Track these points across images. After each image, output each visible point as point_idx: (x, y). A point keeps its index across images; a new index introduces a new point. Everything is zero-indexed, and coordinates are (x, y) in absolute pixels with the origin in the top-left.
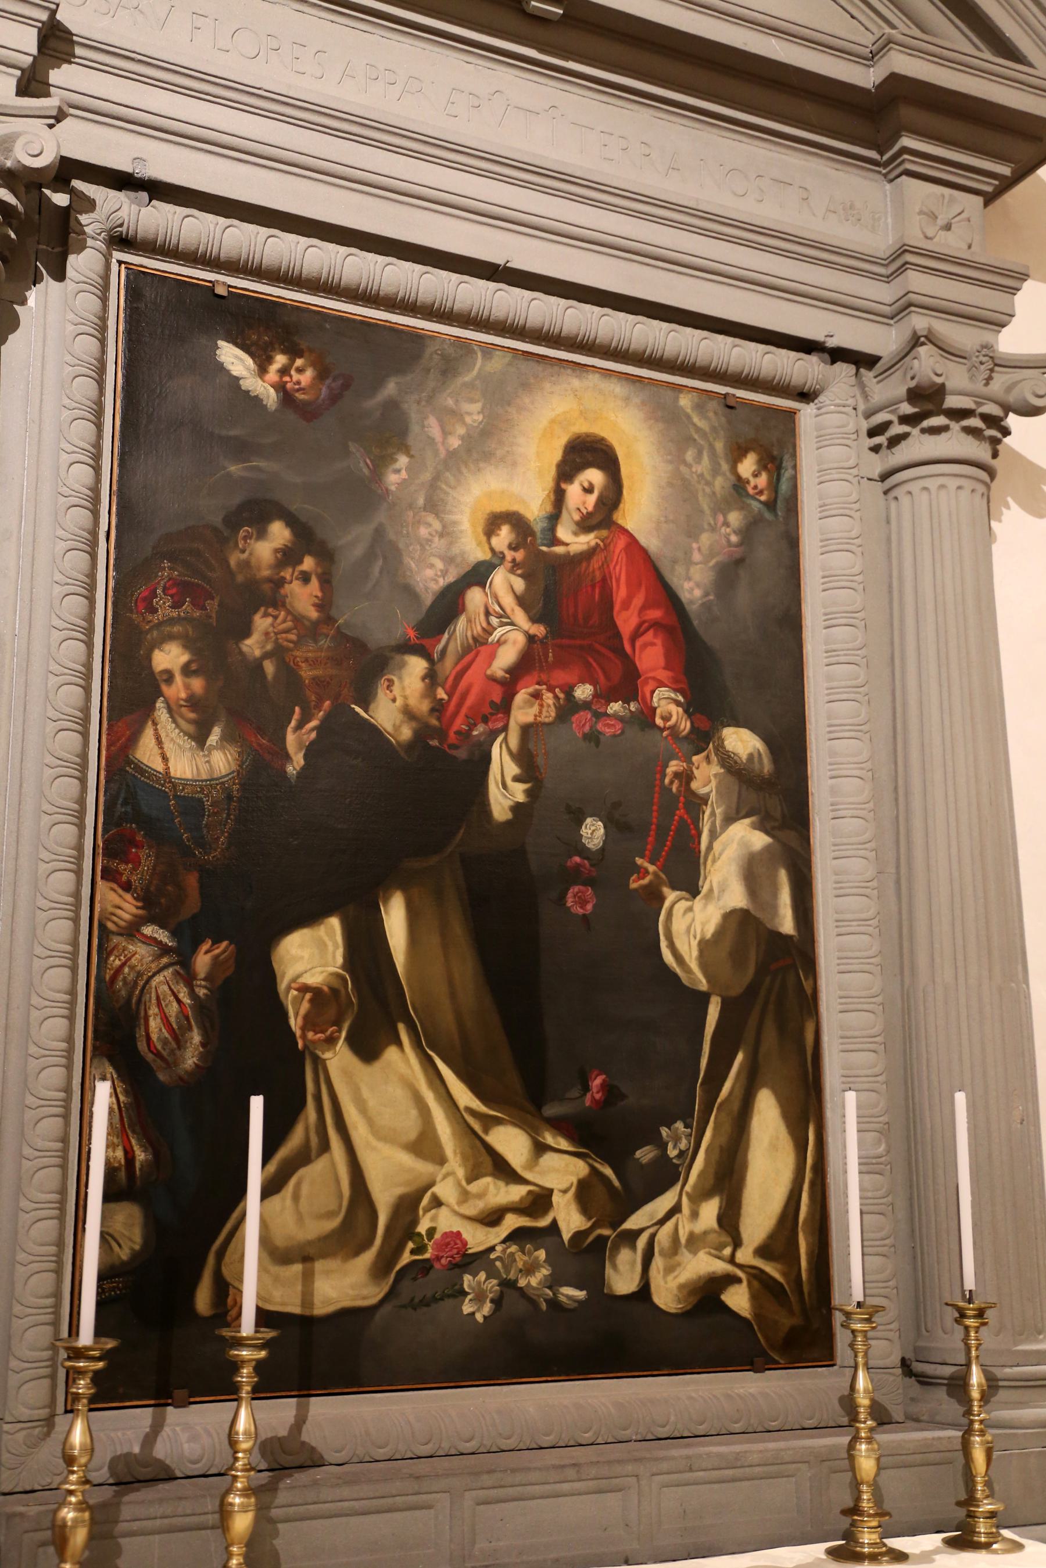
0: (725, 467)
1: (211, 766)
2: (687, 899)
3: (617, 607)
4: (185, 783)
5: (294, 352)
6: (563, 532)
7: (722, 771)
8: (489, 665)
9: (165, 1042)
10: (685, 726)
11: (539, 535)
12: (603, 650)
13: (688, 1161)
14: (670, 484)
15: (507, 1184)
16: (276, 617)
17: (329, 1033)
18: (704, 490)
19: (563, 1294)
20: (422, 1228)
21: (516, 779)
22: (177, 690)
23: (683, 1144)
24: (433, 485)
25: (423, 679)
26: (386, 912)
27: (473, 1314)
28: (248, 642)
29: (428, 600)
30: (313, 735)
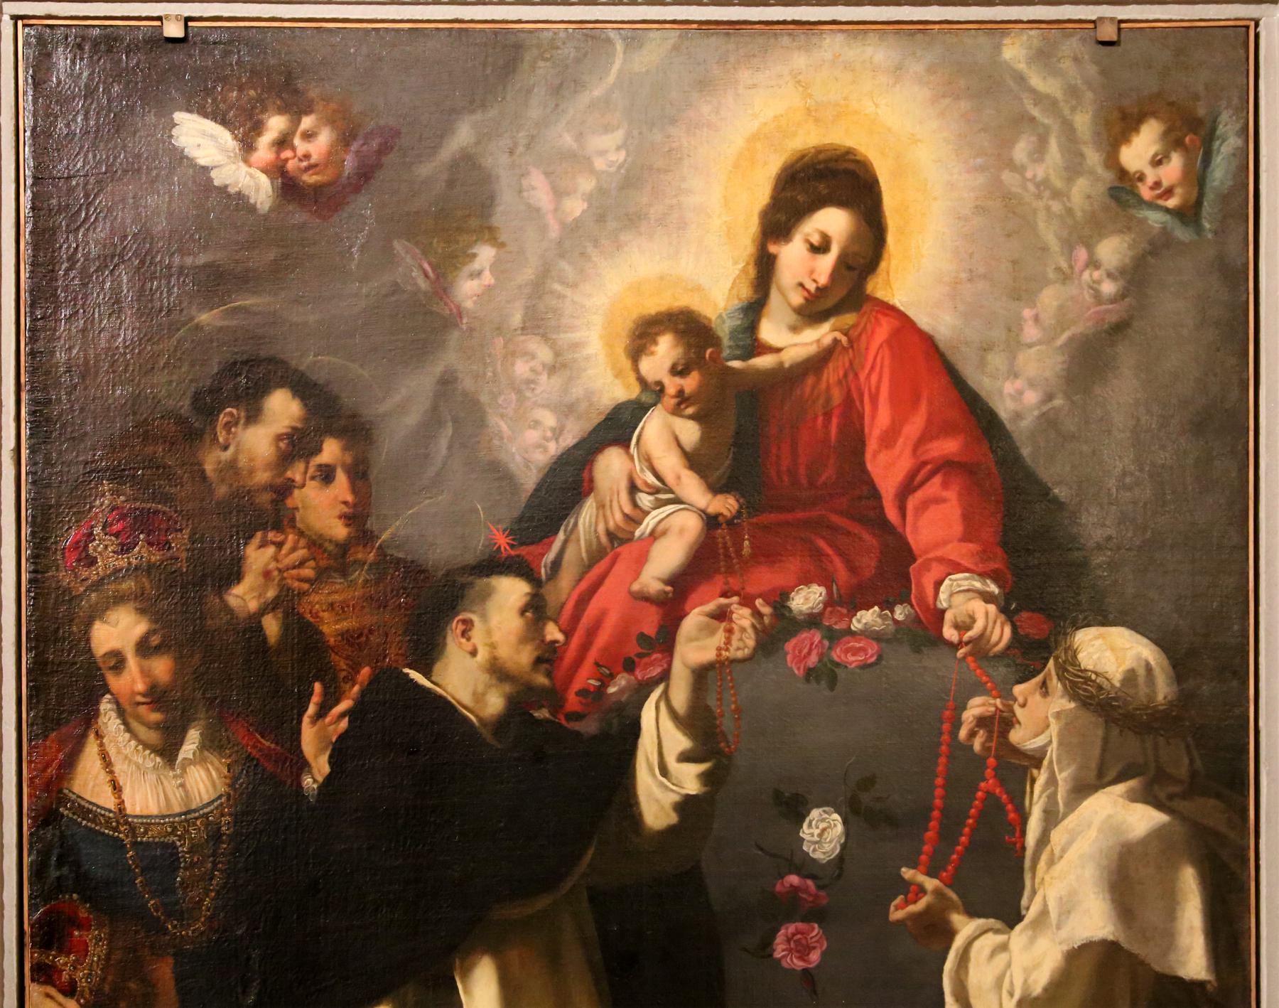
0: (1093, 158)
1: (186, 792)
2: (997, 931)
3: (872, 445)
4: (148, 822)
5: (296, 106)
6: (771, 331)
7: (1073, 705)
8: (637, 574)
10: (1001, 635)
11: (726, 342)
14: (980, 210)
16: (279, 545)
18: (1048, 209)
21: (685, 757)
22: (131, 681)
24: (538, 287)
25: (523, 612)
28: (238, 590)
29: (529, 480)
30: (344, 724)
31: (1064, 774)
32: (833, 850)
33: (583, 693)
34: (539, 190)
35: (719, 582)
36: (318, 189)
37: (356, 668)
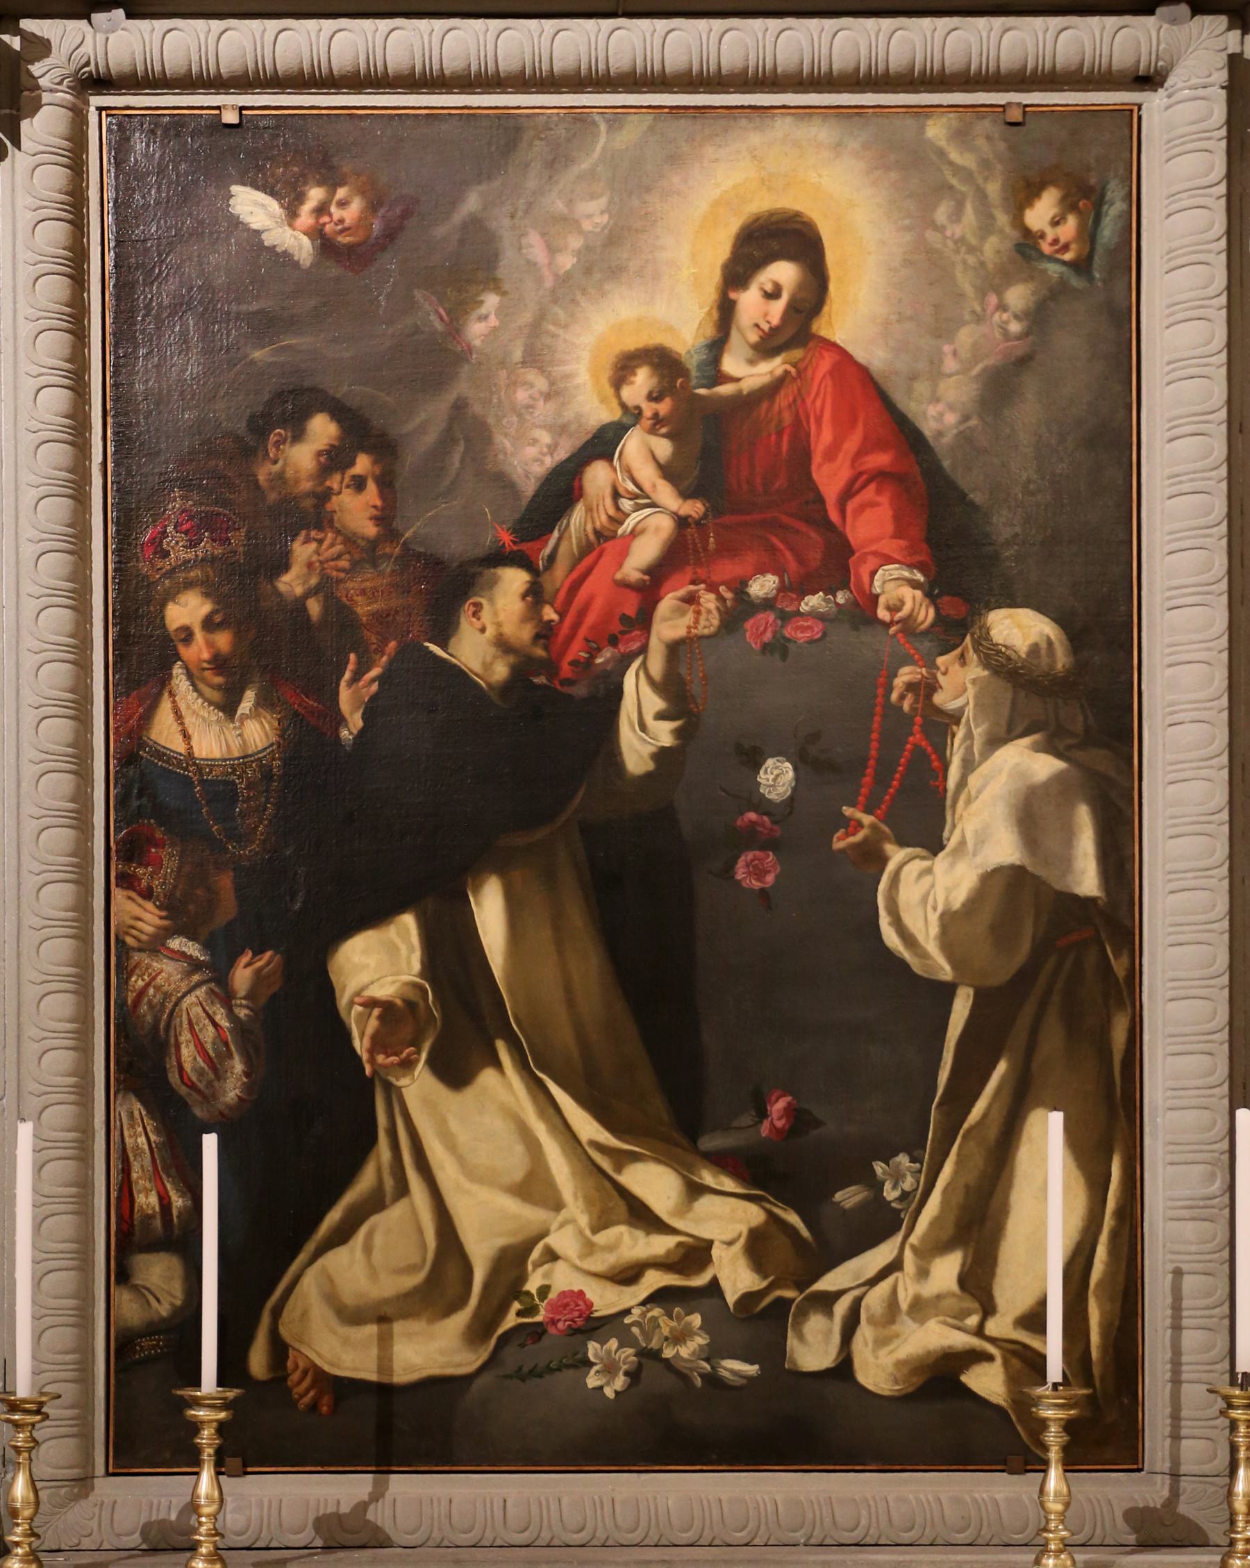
0: (1002, 219)
2: (923, 858)
3: (817, 458)
4: (212, 763)
5: (332, 181)
6: (731, 364)
7: (986, 673)
8: (620, 565)
9: (201, 1073)
10: (927, 615)
11: (694, 373)
12: (796, 524)
13: (914, 1206)
14: (908, 263)
15: (648, 1234)
16: (320, 542)
17: (404, 1055)
18: (964, 262)
19: (726, 1369)
20: (532, 1285)
21: (660, 716)
22: (198, 650)
23: (908, 1183)
24: (536, 328)
25: (524, 596)
26: (477, 904)
27: (601, 1388)
28: (286, 578)
29: (529, 488)
30: (375, 687)
31: (979, 730)
32: (787, 790)
33: (574, 663)
34: (536, 248)
35: (689, 573)
36: (351, 248)
37: (385, 642)
